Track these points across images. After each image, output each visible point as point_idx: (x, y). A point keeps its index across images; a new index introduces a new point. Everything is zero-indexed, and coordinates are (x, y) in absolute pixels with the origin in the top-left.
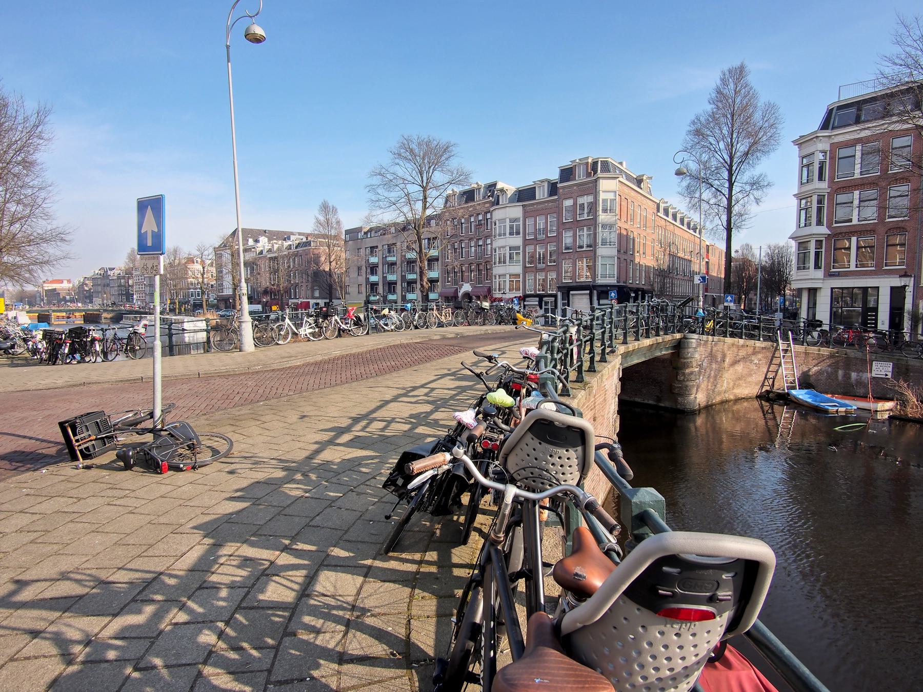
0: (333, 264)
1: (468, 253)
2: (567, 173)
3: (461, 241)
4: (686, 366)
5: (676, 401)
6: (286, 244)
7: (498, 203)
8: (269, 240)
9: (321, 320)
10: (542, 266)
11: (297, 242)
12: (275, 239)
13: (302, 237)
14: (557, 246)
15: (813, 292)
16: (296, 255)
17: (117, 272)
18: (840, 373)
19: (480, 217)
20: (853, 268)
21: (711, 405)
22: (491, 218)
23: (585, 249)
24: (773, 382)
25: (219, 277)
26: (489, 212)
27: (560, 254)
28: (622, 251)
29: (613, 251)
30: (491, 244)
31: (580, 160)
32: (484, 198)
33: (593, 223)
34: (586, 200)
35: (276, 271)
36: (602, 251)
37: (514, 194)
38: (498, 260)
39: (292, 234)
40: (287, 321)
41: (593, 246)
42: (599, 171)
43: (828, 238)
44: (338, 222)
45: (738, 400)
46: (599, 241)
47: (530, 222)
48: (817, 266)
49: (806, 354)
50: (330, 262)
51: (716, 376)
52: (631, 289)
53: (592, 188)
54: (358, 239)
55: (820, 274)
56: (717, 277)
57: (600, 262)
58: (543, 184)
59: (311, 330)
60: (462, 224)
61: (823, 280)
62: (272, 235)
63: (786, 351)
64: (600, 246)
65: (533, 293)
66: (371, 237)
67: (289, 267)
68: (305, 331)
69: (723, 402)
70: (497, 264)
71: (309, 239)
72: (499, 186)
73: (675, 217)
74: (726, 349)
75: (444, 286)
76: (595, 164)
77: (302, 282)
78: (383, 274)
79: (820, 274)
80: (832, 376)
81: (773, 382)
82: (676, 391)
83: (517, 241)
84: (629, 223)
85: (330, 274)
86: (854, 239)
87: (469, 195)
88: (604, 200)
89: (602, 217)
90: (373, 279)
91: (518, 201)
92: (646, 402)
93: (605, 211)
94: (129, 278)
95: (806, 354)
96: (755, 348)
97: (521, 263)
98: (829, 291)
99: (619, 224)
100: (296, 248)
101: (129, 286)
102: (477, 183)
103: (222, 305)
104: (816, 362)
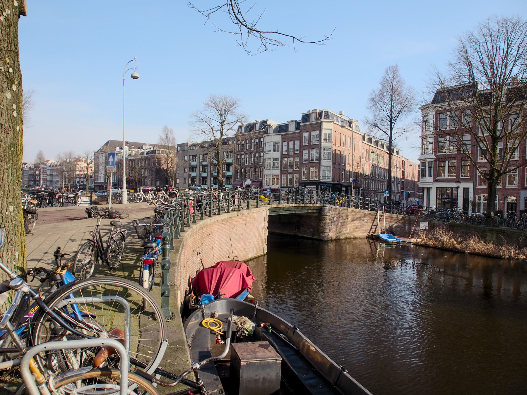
0: (170, 165)
1: (250, 161)
2: (306, 117)
3: (246, 154)
4: (324, 219)
5: (320, 236)
6: (140, 151)
7: (267, 133)
8: (130, 149)
9: (156, 193)
10: (291, 170)
11: (148, 150)
12: (133, 148)
13: (150, 147)
14: (300, 159)
15: (429, 189)
16: (146, 158)
17: (28, 166)
18: (407, 227)
19: (257, 140)
20: (446, 177)
21: (340, 239)
22: (263, 141)
23: (314, 161)
24: (375, 230)
25: (96, 171)
26: (262, 137)
27: (301, 164)
28: (337, 163)
29: (330, 163)
30: (263, 156)
31: (312, 110)
32: (260, 129)
33: (319, 147)
34: (315, 133)
35: (134, 168)
36: (323, 163)
37: (277, 128)
38: (266, 166)
39: (145, 144)
40: (141, 192)
41: (319, 159)
42: (323, 117)
43: (435, 160)
44: (173, 139)
45: (355, 238)
46: (322, 157)
47: (285, 144)
48: (430, 176)
49: (391, 217)
50: (167, 164)
51: (342, 226)
52: (342, 186)
53: (318, 127)
54: (185, 150)
55: (431, 180)
56: (412, 181)
57: (322, 169)
58: (293, 123)
59: (152, 197)
60: (247, 144)
61: (433, 183)
62: (131, 145)
63: (382, 216)
64: (322, 160)
65: (285, 186)
66: (193, 149)
67: (142, 166)
68: (149, 197)
69: (346, 239)
70: (266, 169)
71: (155, 149)
72: (268, 123)
73: (377, 143)
74: (348, 213)
75: (235, 181)
76: (321, 113)
77: (149, 176)
78: (199, 172)
79: (431, 180)
80: (403, 228)
81: (375, 230)
82: (320, 231)
83: (278, 155)
84: (341, 147)
85: (166, 171)
86: (447, 162)
87: (251, 127)
88: (324, 134)
89: (324, 144)
90: (193, 175)
91: (279, 132)
92: (308, 236)
93: (325, 140)
94: (36, 170)
95: (391, 217)
96: (365, 214)
97: (280, 168)
98: (436, 189)
99: (334, 147)
100: (147, 154)
101: (36, 175)
102: (256, 120)
103: (97, 189)
104: (395, 221)
